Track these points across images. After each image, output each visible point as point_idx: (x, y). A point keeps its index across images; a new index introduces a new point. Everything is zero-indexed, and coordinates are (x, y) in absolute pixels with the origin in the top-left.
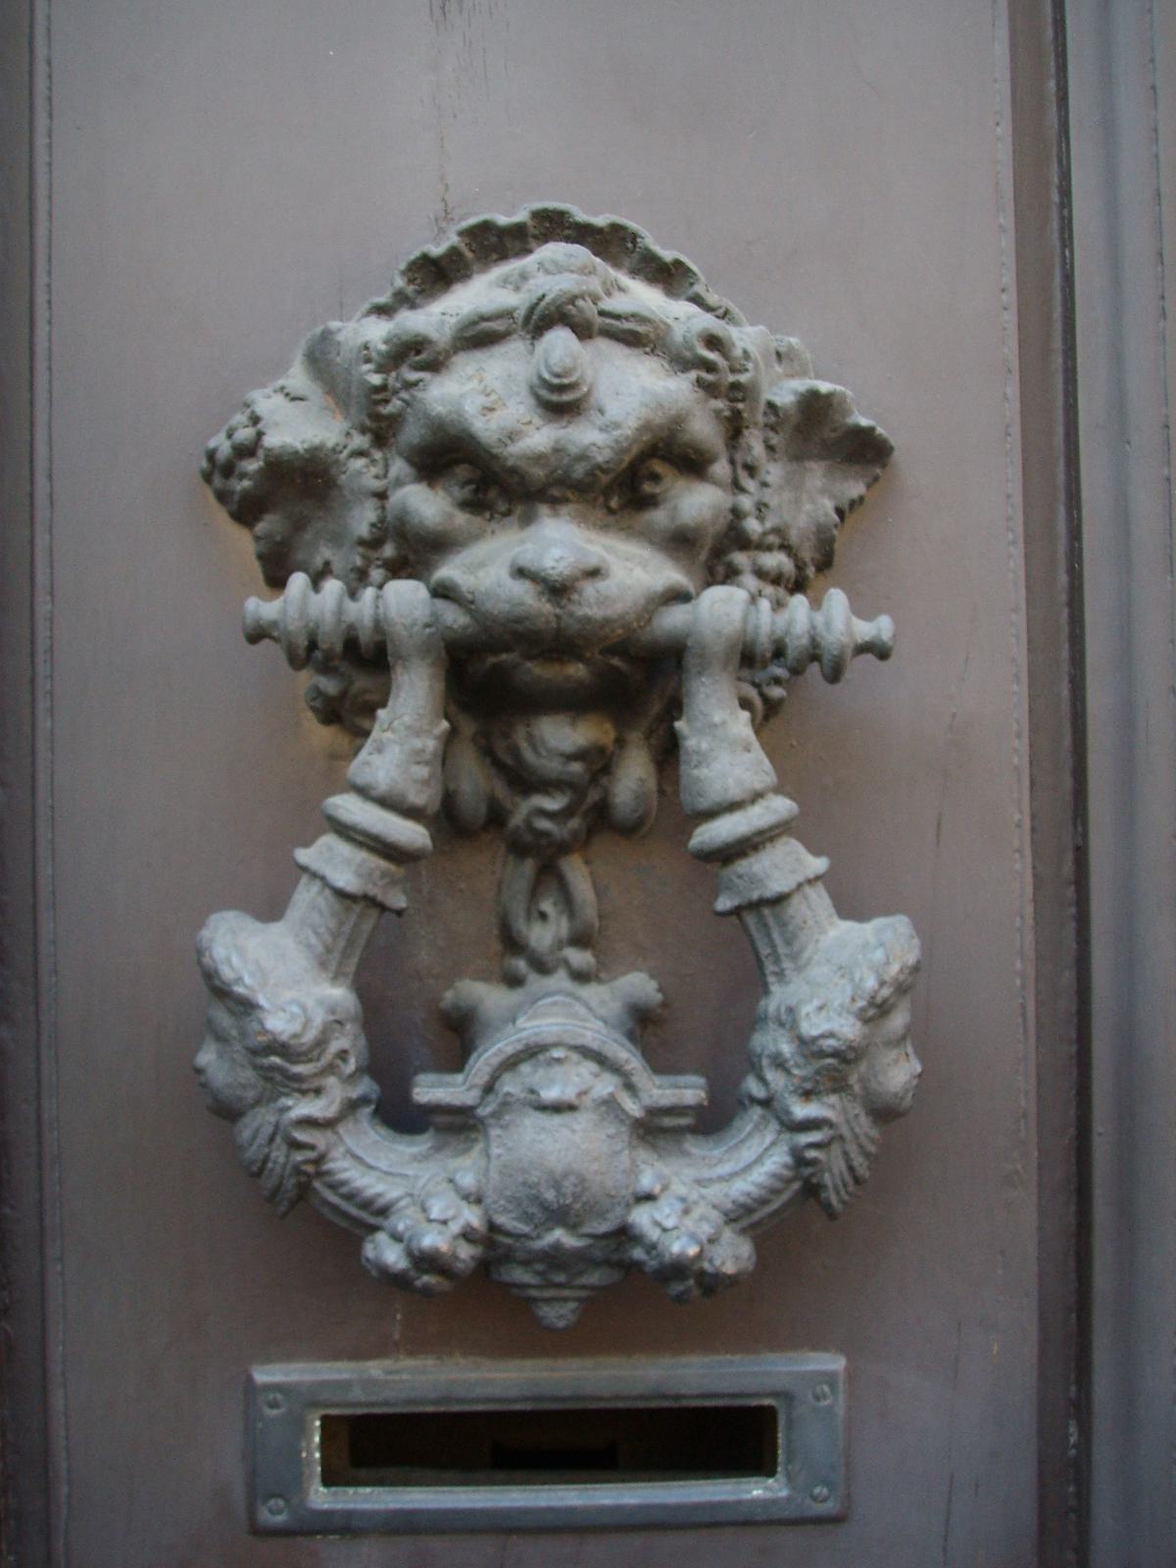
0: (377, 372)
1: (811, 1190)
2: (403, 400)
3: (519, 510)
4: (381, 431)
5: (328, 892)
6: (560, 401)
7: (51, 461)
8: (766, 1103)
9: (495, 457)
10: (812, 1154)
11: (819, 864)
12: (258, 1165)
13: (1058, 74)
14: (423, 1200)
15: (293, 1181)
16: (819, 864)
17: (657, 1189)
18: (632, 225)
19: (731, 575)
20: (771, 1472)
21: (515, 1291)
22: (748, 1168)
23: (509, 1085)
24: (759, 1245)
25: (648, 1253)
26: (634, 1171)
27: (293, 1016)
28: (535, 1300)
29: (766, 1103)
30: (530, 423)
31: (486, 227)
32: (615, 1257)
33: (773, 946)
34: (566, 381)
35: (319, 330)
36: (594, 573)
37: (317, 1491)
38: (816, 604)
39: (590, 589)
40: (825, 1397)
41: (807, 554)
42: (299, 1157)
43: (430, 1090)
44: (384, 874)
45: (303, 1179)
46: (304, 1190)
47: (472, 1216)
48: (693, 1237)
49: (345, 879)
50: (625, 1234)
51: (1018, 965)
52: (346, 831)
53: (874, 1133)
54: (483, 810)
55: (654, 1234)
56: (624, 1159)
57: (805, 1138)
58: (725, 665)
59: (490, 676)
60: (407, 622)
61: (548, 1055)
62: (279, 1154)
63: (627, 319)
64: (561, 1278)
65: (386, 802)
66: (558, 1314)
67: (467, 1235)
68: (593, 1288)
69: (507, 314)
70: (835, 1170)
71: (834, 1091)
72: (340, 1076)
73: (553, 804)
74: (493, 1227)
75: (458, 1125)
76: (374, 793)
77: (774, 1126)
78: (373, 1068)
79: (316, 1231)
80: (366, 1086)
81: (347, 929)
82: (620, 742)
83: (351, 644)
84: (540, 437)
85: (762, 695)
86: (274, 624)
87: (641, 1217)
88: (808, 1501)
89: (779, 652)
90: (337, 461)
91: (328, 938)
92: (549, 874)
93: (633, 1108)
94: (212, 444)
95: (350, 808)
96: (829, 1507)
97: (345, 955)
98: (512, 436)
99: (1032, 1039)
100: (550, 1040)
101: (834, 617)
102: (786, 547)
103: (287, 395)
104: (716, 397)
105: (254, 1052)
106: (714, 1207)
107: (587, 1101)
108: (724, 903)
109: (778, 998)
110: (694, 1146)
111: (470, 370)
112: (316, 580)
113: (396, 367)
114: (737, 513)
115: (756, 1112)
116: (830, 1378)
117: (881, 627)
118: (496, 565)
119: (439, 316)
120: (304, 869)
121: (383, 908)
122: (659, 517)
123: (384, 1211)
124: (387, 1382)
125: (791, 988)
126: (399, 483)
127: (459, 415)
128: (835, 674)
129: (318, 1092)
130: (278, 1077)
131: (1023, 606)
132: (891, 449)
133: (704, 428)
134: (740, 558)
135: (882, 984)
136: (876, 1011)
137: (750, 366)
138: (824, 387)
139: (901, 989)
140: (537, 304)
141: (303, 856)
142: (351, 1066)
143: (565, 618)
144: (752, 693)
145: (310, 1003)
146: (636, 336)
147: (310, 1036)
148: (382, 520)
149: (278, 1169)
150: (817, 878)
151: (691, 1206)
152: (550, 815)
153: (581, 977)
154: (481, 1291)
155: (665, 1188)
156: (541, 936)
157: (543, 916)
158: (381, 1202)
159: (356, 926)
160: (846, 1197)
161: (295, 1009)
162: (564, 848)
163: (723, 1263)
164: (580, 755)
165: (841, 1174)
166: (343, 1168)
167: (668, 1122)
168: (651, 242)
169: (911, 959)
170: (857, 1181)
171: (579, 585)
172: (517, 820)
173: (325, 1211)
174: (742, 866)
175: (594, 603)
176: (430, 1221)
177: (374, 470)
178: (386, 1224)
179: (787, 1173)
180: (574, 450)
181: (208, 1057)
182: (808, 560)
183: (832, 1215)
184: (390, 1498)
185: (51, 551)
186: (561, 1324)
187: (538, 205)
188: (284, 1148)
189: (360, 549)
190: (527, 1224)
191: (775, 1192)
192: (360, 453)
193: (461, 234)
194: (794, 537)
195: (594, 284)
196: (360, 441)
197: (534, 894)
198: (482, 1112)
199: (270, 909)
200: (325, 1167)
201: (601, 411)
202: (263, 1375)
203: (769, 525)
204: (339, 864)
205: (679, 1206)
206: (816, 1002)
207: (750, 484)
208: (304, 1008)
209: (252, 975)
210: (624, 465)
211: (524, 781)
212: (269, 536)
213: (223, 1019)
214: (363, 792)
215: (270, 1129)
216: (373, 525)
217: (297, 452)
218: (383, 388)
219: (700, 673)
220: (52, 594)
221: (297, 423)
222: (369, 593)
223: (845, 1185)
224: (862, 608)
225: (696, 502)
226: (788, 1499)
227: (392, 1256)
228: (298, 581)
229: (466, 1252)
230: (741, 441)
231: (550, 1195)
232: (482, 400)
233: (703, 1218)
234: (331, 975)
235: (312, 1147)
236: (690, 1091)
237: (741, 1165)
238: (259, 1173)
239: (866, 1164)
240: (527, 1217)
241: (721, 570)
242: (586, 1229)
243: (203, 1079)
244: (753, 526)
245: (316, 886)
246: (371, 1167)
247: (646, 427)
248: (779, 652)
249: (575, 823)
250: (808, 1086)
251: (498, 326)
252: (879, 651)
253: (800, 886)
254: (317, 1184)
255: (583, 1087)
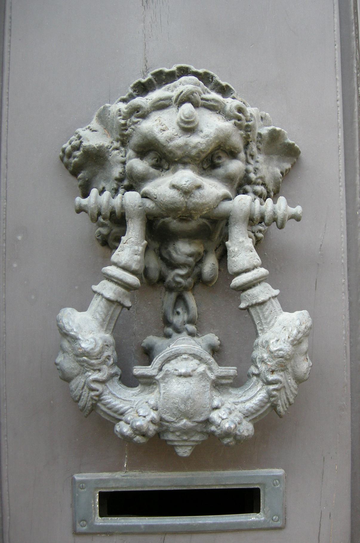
0: (123, 119)
1: (274, 407)
2: (132, 129)
3: (172, 168)
4: (124, 141)
5: (104, 300)
6: (189, 128)
7: (7, 153)
8: (258, 375)
9: (164, 146)
10: (274, 393)
11: (276, 292)
12: (78, 397)
13: (355, 30)
14: (136, 409)
15: (91, 403)
16: (276, 292)
17: (220, 405)
18: (212, 73)
19: (245, 192)
20: (258, 511)
21: (169, 443)
22: (252, 398)
23: (168, 367)
24: (256, 426)
25: (217, 427)
26: (211, 399)
27: (91, 343)
28: (176, 446)
29: (258, 375)
30: (177, 135)
31: (161, 73)
32: (205, 430)
33: (260, 320)
34: (190, 120)
35: (102, 107)
36: (199, 187)
37: (98, 519)
38: (275, 202)
39: (197, 193)
40: (277, 485)
41: (271, 187)
42: (93, 393)
43: (139, 370)
44: (124, 294)
45: (94, 402)
46: (94, 407)
47: (154, 414)
48: (233, 421)
49: (109, 294)
50: (208, 422)
51: (344, 332)
52: (110, 278)
53: (295, 386)
54: (157, 275)
55: (219, 421)
56: (208, 394)
57: (271, 387)
58: (244, 222)
59: (159, 229)
60: (133, 205)
61: (182, 357)
62: (86, 392)
63: (211, 101)
64: (185, 438)
65: (125, 268)
66: (184, 452)
67: (152, 421)
68: (197, 441)
69: (169, 98)
70: (282, 399)
71: (282, 371)
72: (107, 365)
73: (182, 272)
74: (162, 419)
75: (149, 382)
76: (121, 265)
77: (261, 383)
78: (118, 363)
79: (98, 421)
80: (116, 369)
81: (110, 313)
82: (206, 252)
83: (113, 213)
84: (181, 140)
85: (255, 235)
86: (86, 206)
87: (215, 416)
88: (271, 521)
89: (262, 219)
90: (108, 151)
91: (103, 315)
92: (180, 299)
93: (213, 377)
94: (64, 146)
95: (111, 270)
96: (279, 524)
97: (109, 323)
98: (171, 139)
99: (349, 358)
100: (183, 352)
101: (281, 206)
102: (264, 184)
103: (91, 129)
104: (241, 130)
105: (77, 356)
106: (240, 412)
107: (195, 373)
108: (243, 305)
109: (262, 338)
110: (233, 391)
111: (156, 118)
112: (101, 192)
113: (130, 117)
114: (247, 171)
115: (255, 378)
116: (278, 478)
117: (298, 210)
118: (164, 187)
119: (144, 101)
120: (95, 292)
121: (123, 306)
122: (220, 171)
123: (122, 414)
124: (123, 479)
125: (267, 335)
126: (130, 158)
127: (152, 132)
128: (281, 227)
129: (99, 370)
130: (86, 365)
131: (345, 208)
132: (300, 152)
133: (237, 140)
134: (248, 187)
135: (299, 332)
136: (296, 343)
137: (253, 119)
138: (278, 129)
139: (306, 335)
140: (180, 95)
141: (95, 288)
142: (111, 362)
143: (189, 202)
144: (252, 235)
145: (97, 338)
146: (214, 108)
147: (97, 349)
148: (124, 171)
149: (85, 399)
150: (276, 296)
151: (232, 412)
152: (182, 276)
153: (191, 334)
154: (155, 445)
155: (223, 405)
156: (177, 320)
157: (178, 313)
158: (122, 410)
159: (114, 311)
160: (286, 409)
161: (92, 340)
162: (186, 289)
163: (243, 431)
164: (191, 255)
165: (284, 400)
166: (108, 398)
167: (224, 381)
168: (218, 78)
169: (309, 324)
170: (290, 404)
171: (193, 191)
172: (169, 279)
173: (102, 414)
174: (249, 292)
175: (197, 198)
176: (140, 416)
177: (121, 154)
178: (123, 418)
179: (266, 400)
180: (192, 145)
181: (59, 359)
182: (271, 189)
183: (281, 416)
184: (123, 521)
185: (6, 184)
186: (185, 455)
187: (179, 65)
188: (88, 390)
189: (116, 182)
190: (174, 418)
191: (262, 407)
192: (117, 149)
193: (152, 75)
194: (267, 180)
195: (199, 89)
196: (116, 144)
197: (175, 306)
198: (158, 377)
199: (83, 307)
200: (102, 398)
201: (202, 131)
202: (78, 477)
203: (258, 176)
204: (108, 289)
205: (228, 411)
206: (276, 339)
207: (252, 162)
208: (95, 339)
209: (77, 328)
210: (209, 151)
211: (172, 265)
212: (83, 178)
213: (66, 344)
214: (115, 264)
215: (83, 384)
216: (121, 173)
217: (94, 148)
218: (125, 125)
219: (234, 225)
220: (6, 199)
221: (94, 138)
222: (120, 195)
223: (286, 404)
224: (291, 203)
225: (235, 166)
226: (265, 521)
227: (124, 428)
228: (94, 192)
229: (152, 427)
230: (249, 146)
231: (182, 407)
232: (160, 127)
233: (236, 416)
234: (104, 329)
235: (98, 391)
236: (232, 371)
237: (249, 397)
238: (78, 401)
239: (293, 397)
240: (174, 415)
241: (241, 191)
242: (196, 420)
243: (58, 367)
244: (252, 176)
245: (99, 298)
246: (118, 398)
247: (217, 137)
248: (262, 219)
249: (190, 280)
250: (273, 368)
251: (166, 102)
252: (296, 218)
253: (270, 298)
254: (99, 404)
255: (194, 368)
